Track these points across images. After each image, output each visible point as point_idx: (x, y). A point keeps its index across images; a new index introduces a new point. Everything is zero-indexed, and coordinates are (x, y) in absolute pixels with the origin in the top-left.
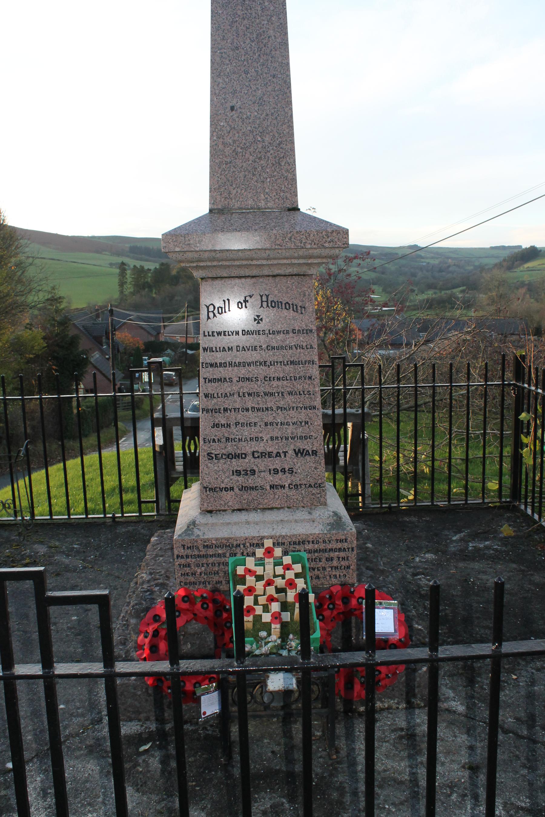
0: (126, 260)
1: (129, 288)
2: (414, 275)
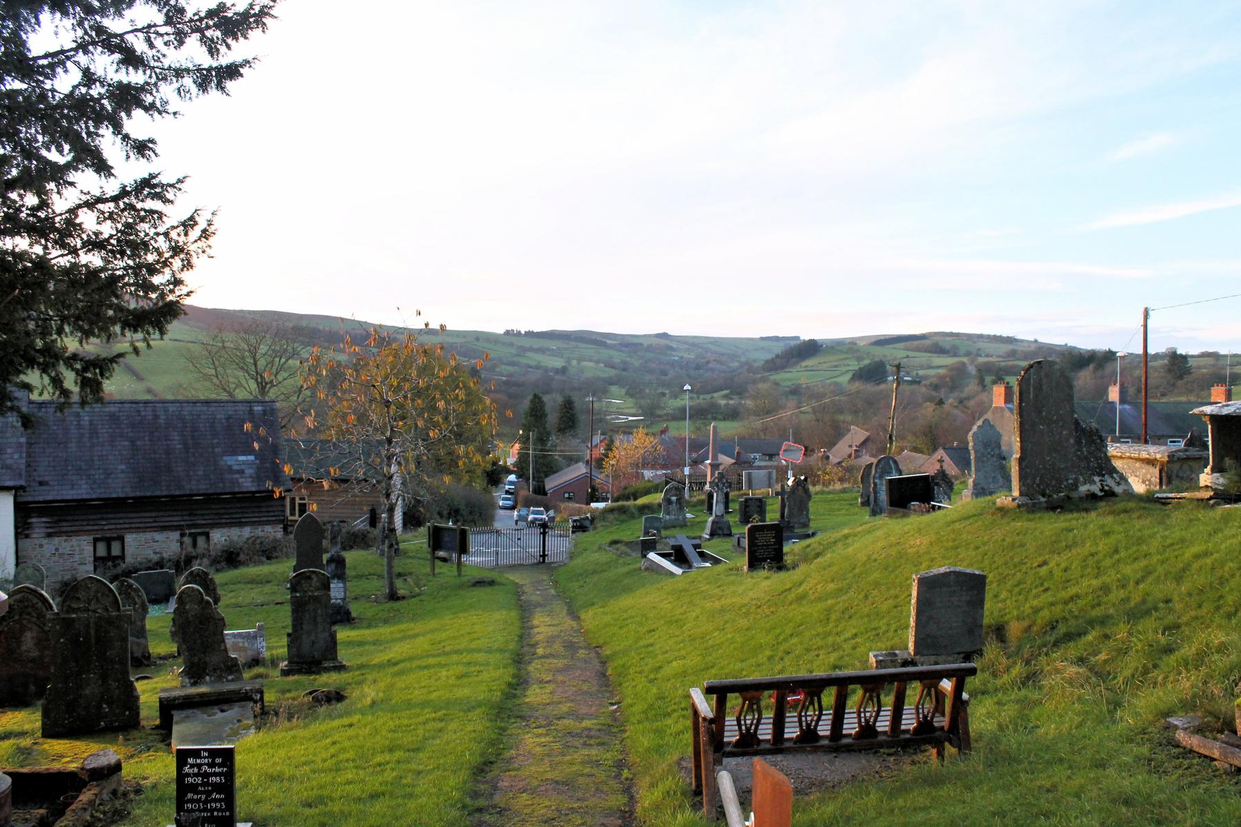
2: (664, 373)
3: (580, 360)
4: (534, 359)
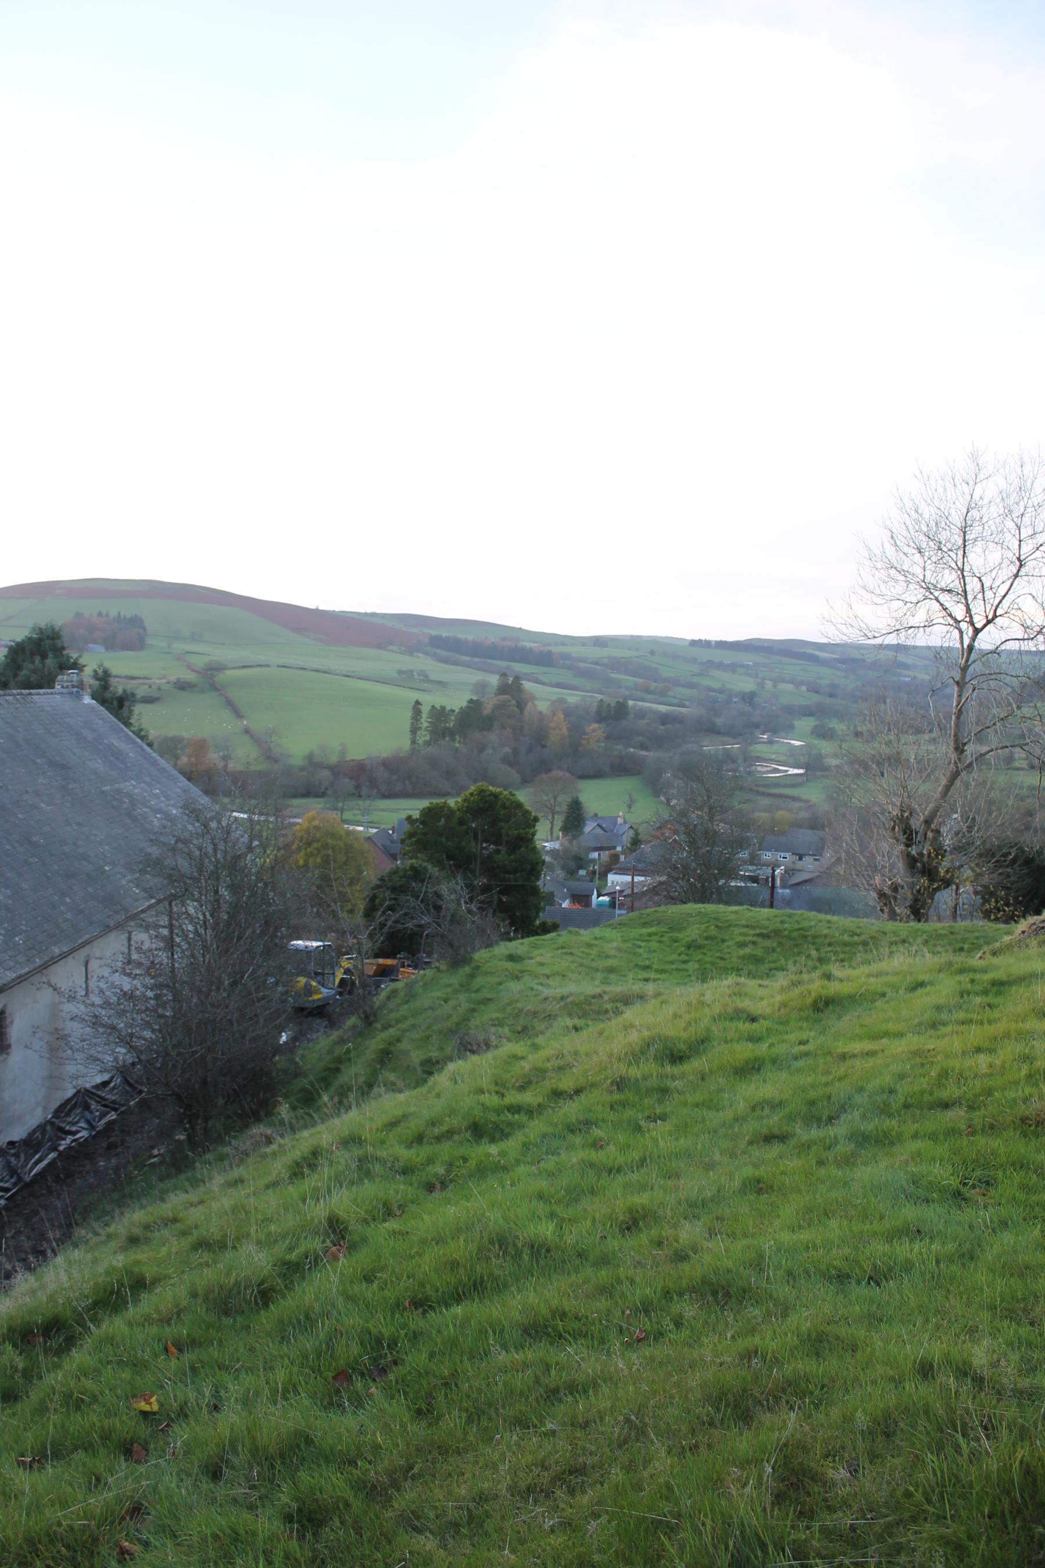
0: (421, 697)
1: (423, 736)
3: (776, 682)
4: (717, 679)
